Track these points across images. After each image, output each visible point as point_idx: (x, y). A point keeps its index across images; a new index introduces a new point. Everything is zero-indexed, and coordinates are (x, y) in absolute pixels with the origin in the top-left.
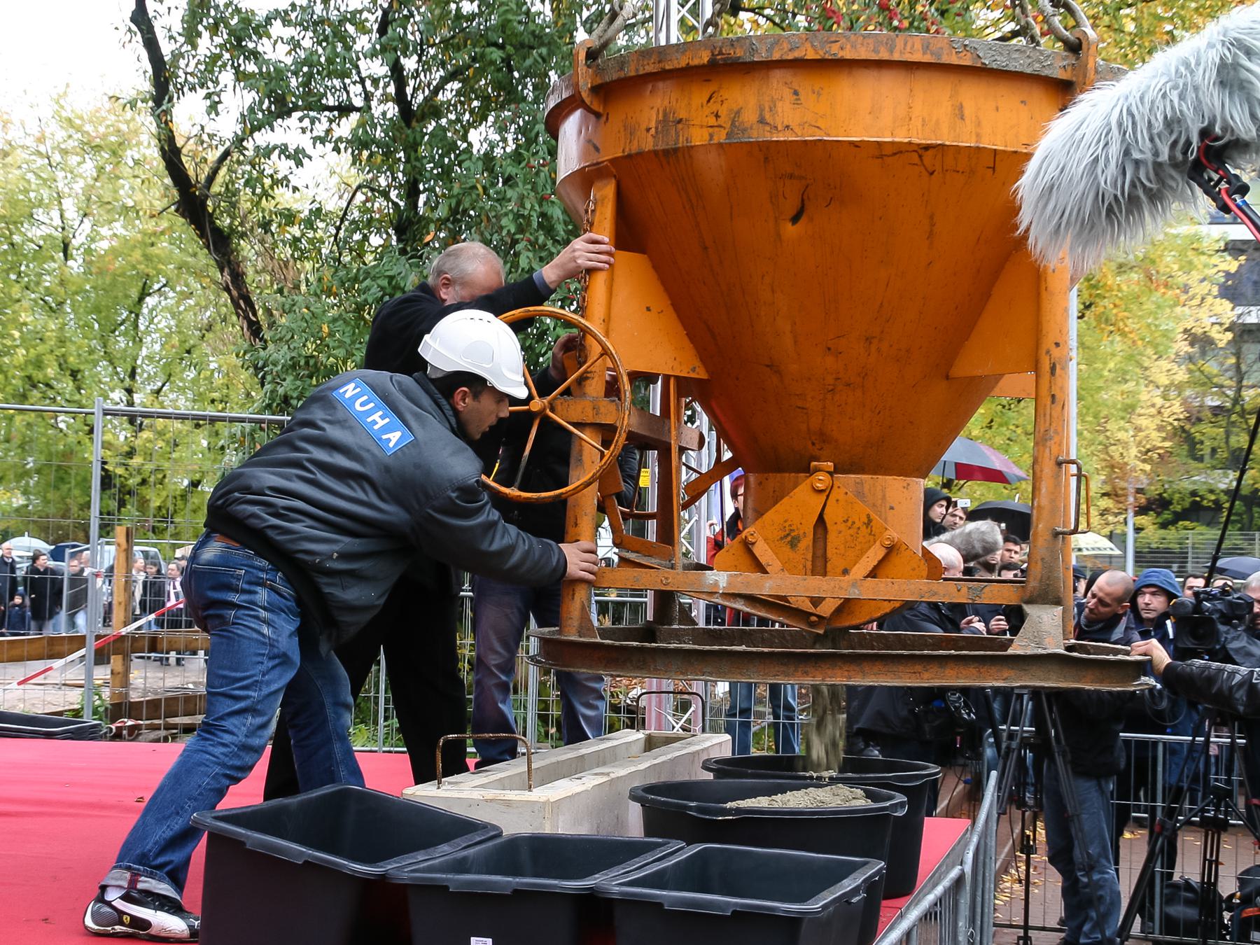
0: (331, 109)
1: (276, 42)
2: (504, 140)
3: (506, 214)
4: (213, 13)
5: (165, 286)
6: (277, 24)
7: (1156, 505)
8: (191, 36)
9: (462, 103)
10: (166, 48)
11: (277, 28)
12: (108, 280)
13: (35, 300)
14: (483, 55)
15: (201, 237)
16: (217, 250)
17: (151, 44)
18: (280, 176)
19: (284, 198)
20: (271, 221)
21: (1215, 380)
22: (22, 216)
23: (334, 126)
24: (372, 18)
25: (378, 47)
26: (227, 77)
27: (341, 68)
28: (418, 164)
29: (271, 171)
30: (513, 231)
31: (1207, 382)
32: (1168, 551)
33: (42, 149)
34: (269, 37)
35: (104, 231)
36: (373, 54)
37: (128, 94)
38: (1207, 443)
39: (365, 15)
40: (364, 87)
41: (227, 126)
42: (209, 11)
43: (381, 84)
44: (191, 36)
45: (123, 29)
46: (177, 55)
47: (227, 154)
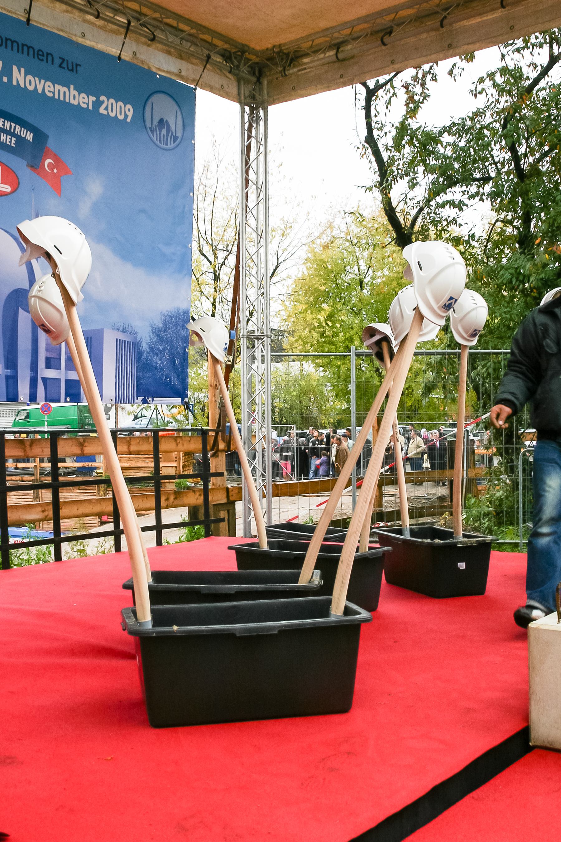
0: (478, 180)
8: (398, 146)
10: (385, 156)
12: (381, 296)
13: (348, 310)
18: (451, 218)
22: (340, 270)
26: (421, 169)
28: (529, 202)
29: (446, 217)
33: (348, 238)
35: (379, 274)
37: (369, 184)
40: (496, 166)
41: (420, 193)
44: (398, 146)
45: (361, 147)
47: (421, 210)
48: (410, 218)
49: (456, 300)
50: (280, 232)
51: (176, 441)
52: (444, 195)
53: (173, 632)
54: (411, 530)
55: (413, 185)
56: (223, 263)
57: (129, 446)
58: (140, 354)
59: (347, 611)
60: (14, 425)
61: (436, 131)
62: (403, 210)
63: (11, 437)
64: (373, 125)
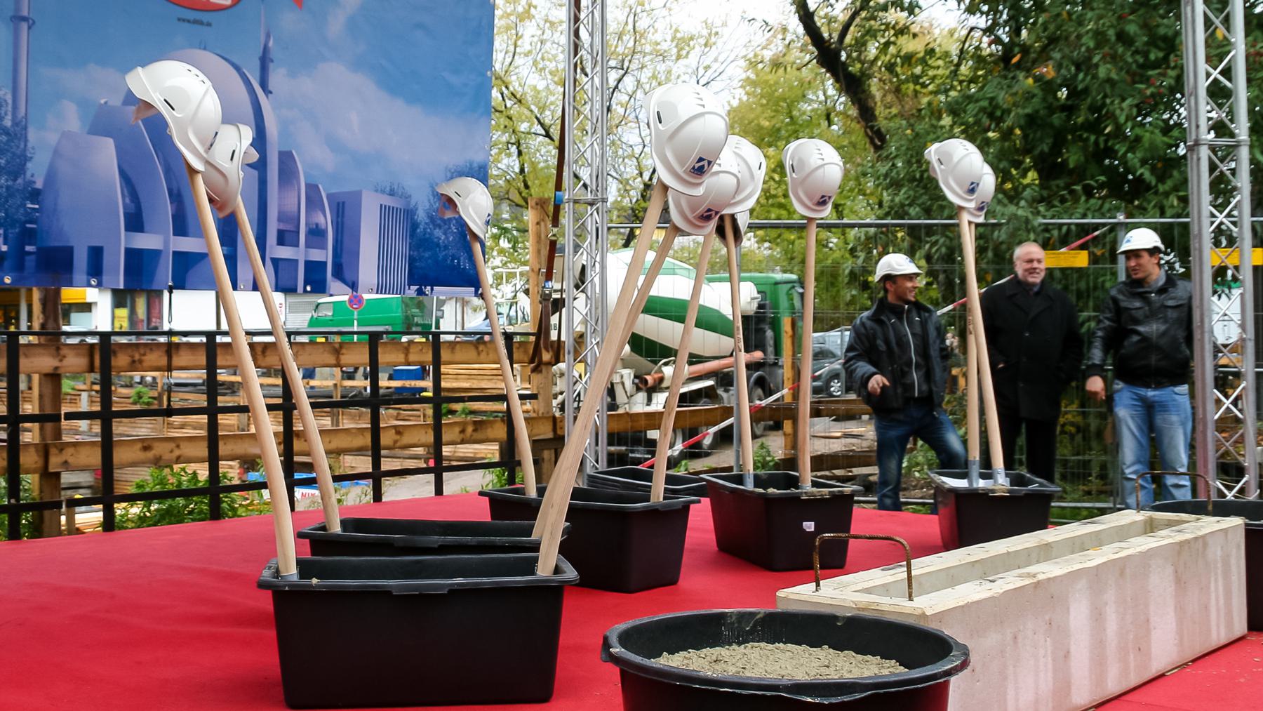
48: (837, 27)
49: (710, 163)
50: (702, 41)
51: (477, 348)
53: (311, 586)
54: (756, 477)
56: (616, 87)
57: (407, 355)
58: (414, 226)
59: (557, 570)
60: (310, 325)
62: (826, 16)
63: (124, 340)
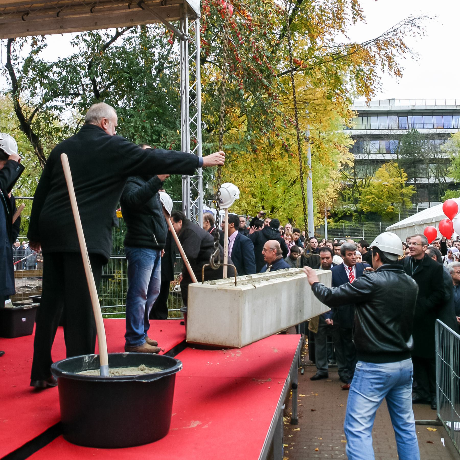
1: (54, 73)
2: (129, 104)
3: (131, 127)
4: (33, 64)
5: (22, 154)
6: (55, 67)
7: (333, 215)
8: (26, 71)
9: (116, 92)
10: (17, 75)
11: (55, 69)
14: (122, 76)
15: (28, 137)
16: (33, 141)
17: (12, 74)
18: (55, 116)
19: (56, 124)
20: (52, 132)
21: (348, 177)
23: (73, 100)
24: (86, 65)
25: (88, 74)
26: (37, 85)
27: (76, 81)
30: (133, 132)
31: (346, 177)
32: (337, 229)
34: (52, 71)
36: (86, 76)
38: (347, 196)
39: (84, 64)
40: (83, 87)
41: (37, 100)
42: (32, 63)
43: (89, 86)
44: (26, 71)
45: (3, 69)
46: (21, 78)
47: (37, 109)
48: (30, 115)
52: (52, 102)
55: (33, 95)
61: (49, 64)
64: (11, 57)
